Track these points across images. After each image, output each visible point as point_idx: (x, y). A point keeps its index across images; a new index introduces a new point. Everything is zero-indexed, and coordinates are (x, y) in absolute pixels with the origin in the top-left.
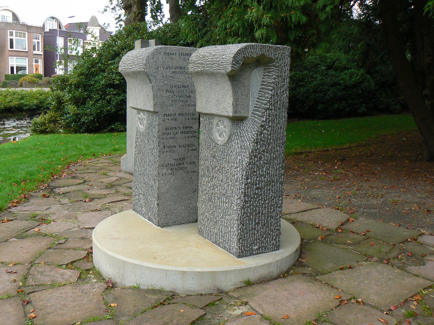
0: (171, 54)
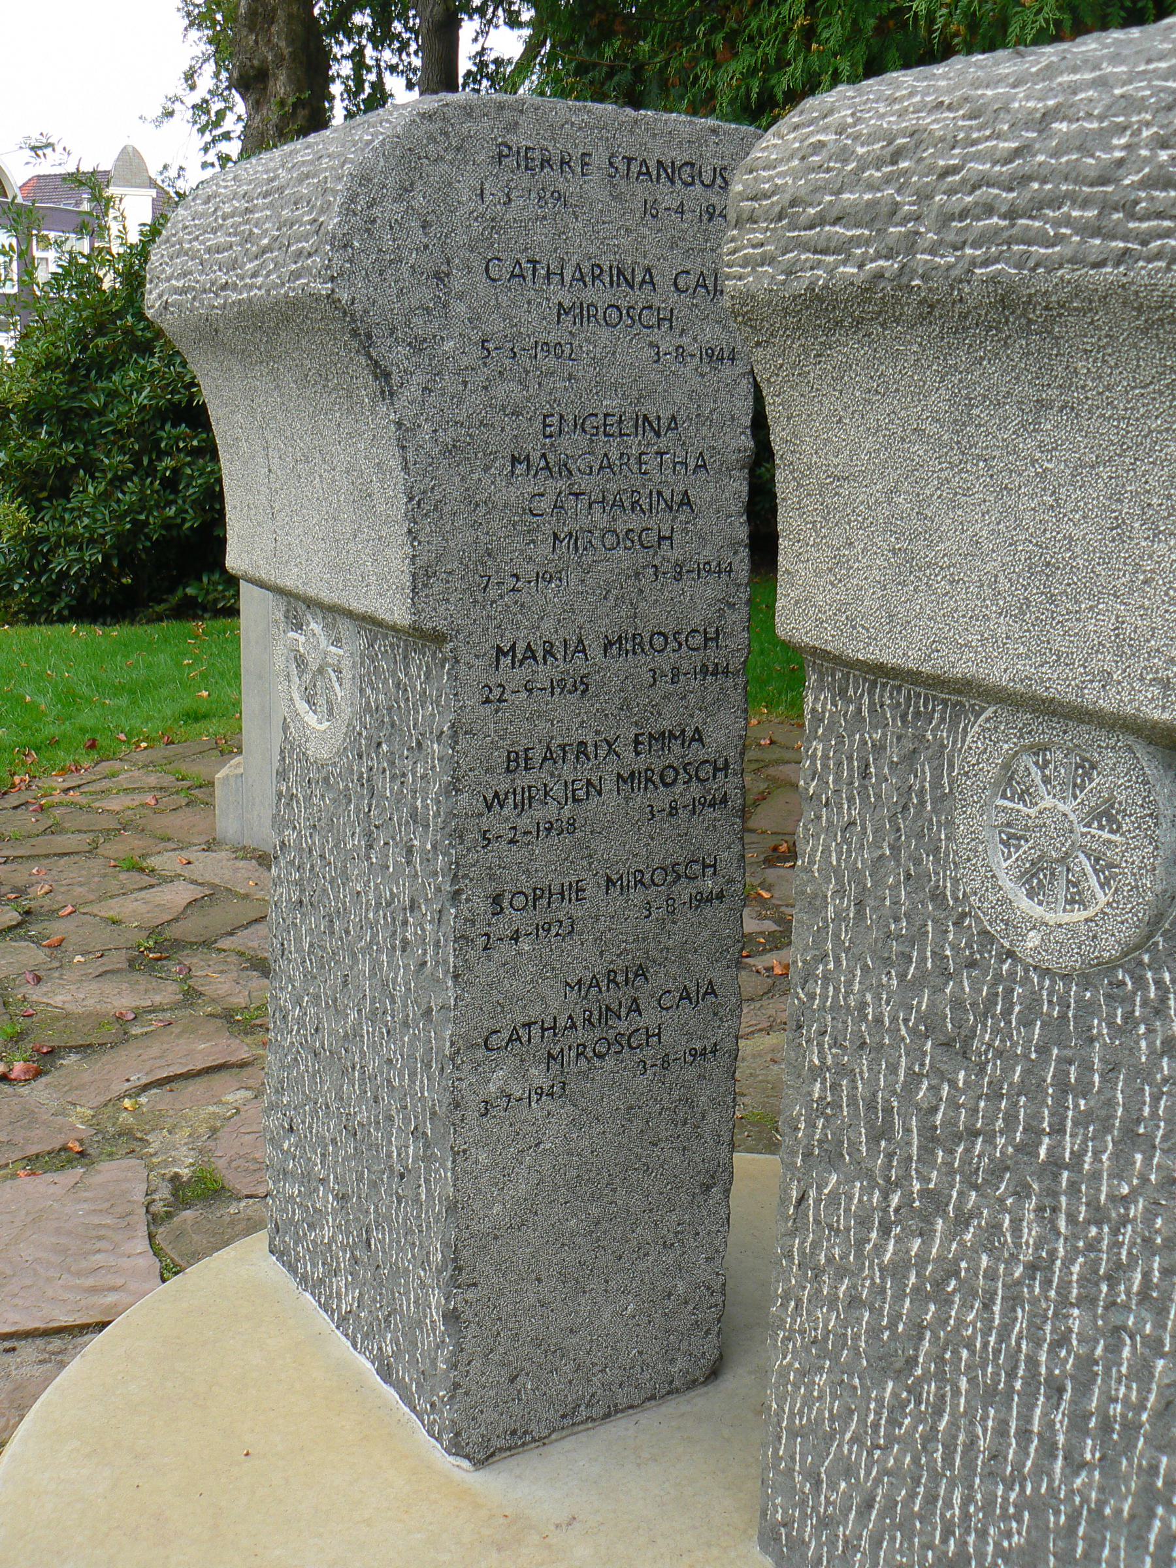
0: (546, 162)
